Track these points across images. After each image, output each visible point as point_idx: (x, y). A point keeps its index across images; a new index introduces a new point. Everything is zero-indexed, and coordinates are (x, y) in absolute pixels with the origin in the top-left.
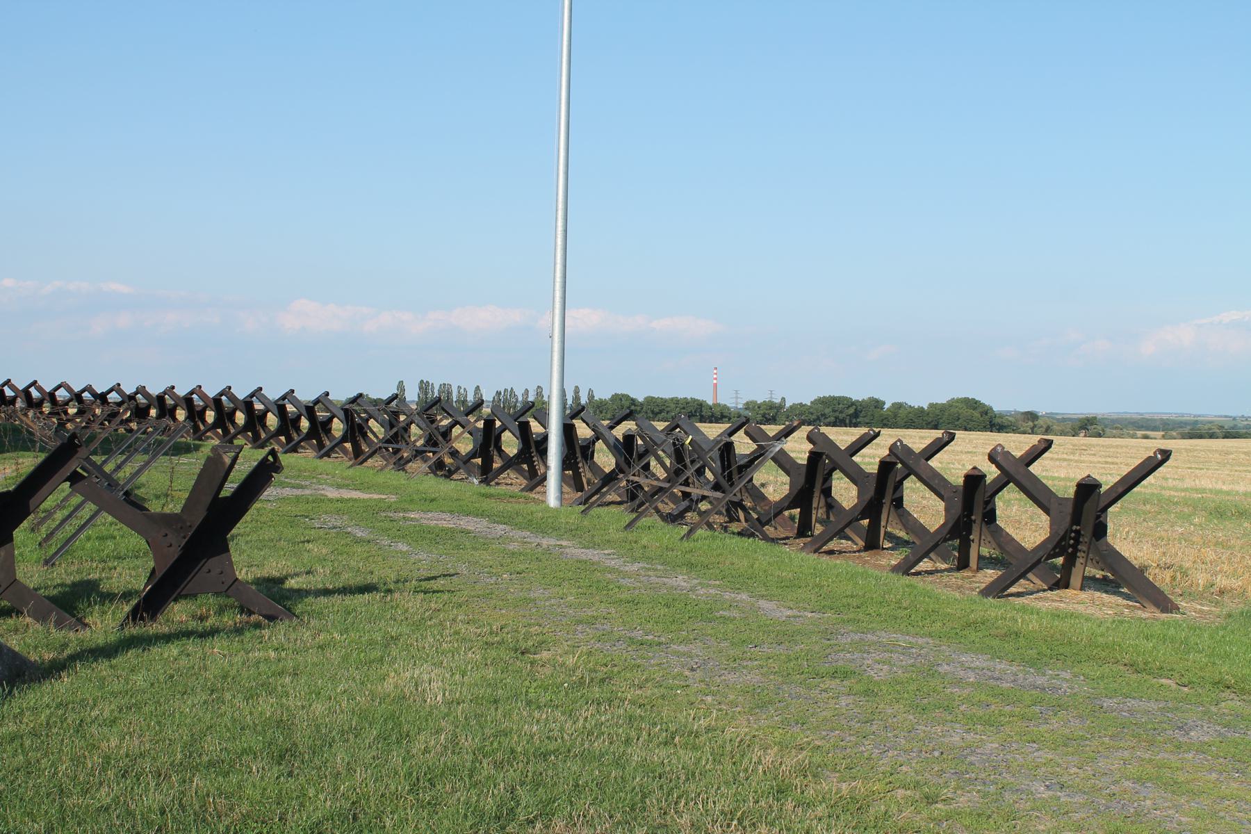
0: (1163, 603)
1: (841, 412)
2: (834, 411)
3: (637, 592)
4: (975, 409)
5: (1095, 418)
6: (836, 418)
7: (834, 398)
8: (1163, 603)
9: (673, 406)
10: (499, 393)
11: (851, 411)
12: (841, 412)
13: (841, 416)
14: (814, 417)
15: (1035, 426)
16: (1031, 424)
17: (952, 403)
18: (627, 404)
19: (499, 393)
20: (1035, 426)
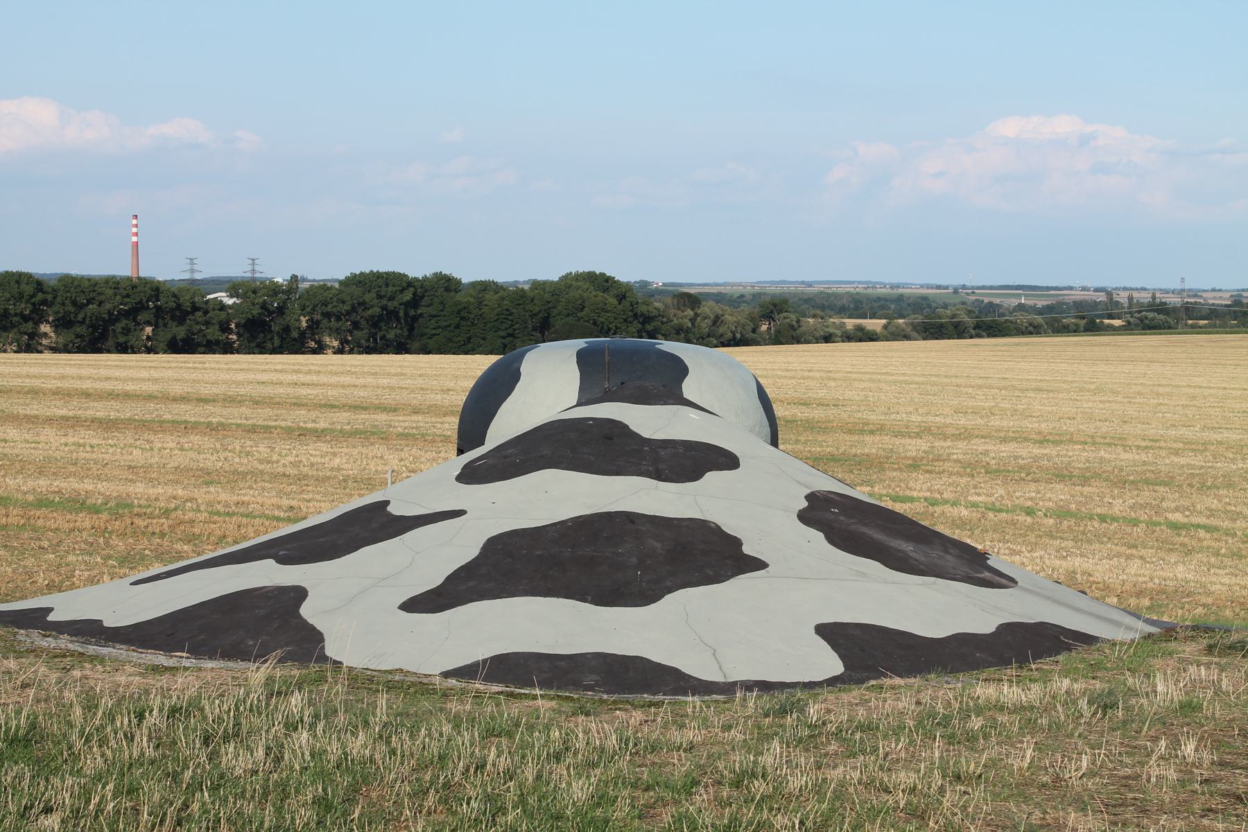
0: (414, 605)
1: (391, 299)
2: (380, 297)
3: (802, 439)
4: (606, 290)
5: (786, 301)
6: (384, 308)
7: (377, 276)
8: (414, 605)
9: (110, 292)
10: (294, 278)
11: (408, 296)
12: (391, 299)
13: (391, 305)
14: (347, 307)
15: (696, 315)
16: (690, 313)
17: (570, 281)
18: (28, 289)
19: (294, 278)
20: (696, 315)
